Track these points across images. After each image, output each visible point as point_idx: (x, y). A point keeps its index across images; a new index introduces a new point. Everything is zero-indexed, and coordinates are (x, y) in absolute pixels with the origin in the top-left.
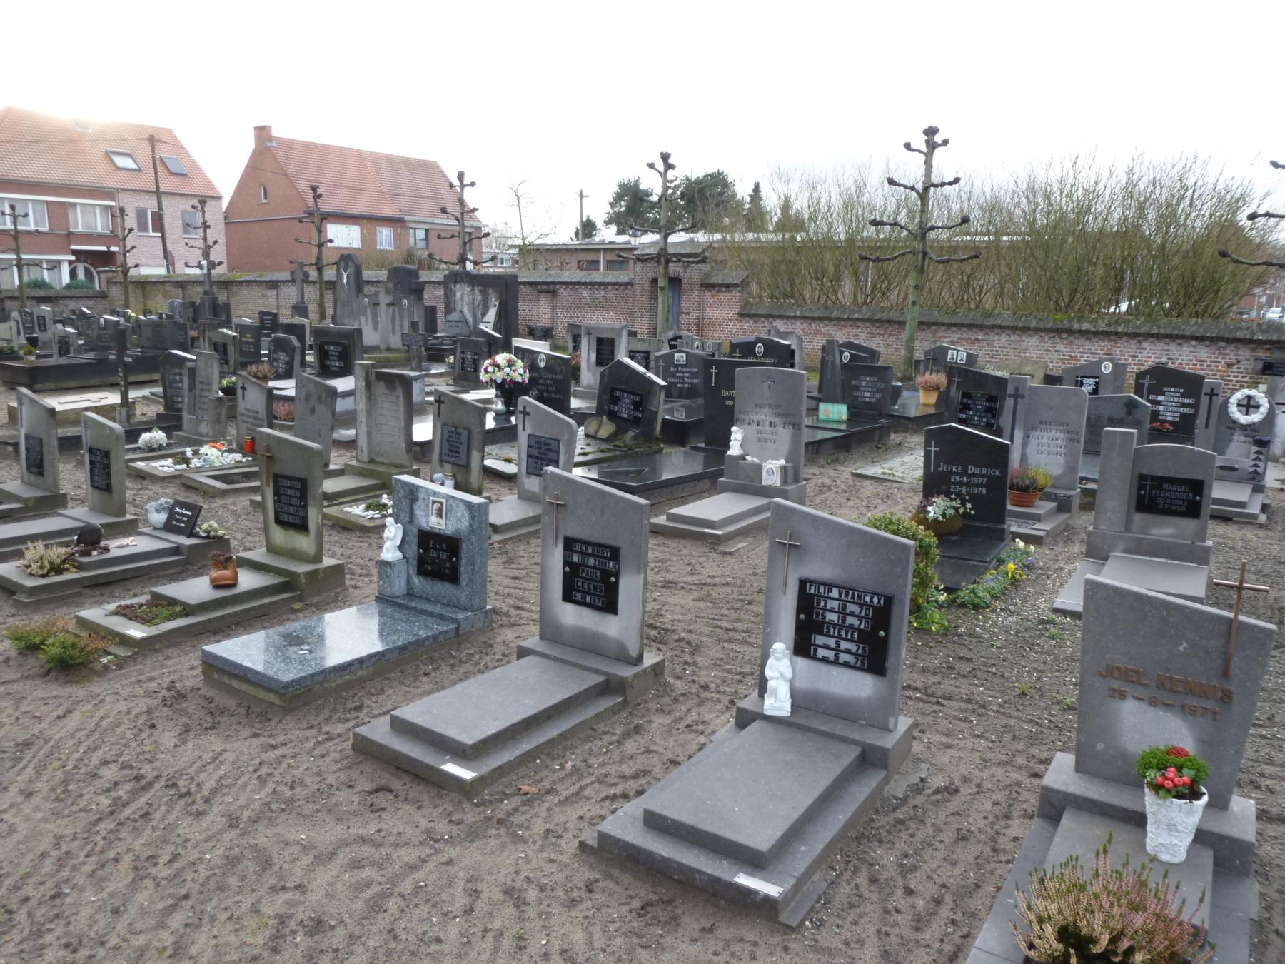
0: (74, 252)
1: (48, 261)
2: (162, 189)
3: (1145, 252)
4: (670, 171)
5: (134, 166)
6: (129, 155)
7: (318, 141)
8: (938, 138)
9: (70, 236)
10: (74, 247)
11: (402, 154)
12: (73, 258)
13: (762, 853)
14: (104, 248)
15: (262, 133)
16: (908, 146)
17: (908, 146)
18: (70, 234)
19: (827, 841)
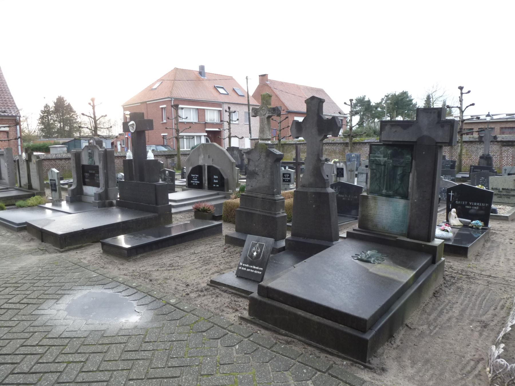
0: (207, 132)
1: (186, 136)
2: (250, 103)
3: (437, 372)
4: (463, 90)
5: (225, 93)
6: (222, 88)
7: (282, 81)
8: (464, 91)
9: (206, 124)
10: (207, 129)
11: (9, 86)
12: (206, 134)
13: (441, 108)
14: (217, 130)
15: (263, 77)
16: (345, 103)
17: (345, 103)
18: (206, 123)
19: (289, 307)
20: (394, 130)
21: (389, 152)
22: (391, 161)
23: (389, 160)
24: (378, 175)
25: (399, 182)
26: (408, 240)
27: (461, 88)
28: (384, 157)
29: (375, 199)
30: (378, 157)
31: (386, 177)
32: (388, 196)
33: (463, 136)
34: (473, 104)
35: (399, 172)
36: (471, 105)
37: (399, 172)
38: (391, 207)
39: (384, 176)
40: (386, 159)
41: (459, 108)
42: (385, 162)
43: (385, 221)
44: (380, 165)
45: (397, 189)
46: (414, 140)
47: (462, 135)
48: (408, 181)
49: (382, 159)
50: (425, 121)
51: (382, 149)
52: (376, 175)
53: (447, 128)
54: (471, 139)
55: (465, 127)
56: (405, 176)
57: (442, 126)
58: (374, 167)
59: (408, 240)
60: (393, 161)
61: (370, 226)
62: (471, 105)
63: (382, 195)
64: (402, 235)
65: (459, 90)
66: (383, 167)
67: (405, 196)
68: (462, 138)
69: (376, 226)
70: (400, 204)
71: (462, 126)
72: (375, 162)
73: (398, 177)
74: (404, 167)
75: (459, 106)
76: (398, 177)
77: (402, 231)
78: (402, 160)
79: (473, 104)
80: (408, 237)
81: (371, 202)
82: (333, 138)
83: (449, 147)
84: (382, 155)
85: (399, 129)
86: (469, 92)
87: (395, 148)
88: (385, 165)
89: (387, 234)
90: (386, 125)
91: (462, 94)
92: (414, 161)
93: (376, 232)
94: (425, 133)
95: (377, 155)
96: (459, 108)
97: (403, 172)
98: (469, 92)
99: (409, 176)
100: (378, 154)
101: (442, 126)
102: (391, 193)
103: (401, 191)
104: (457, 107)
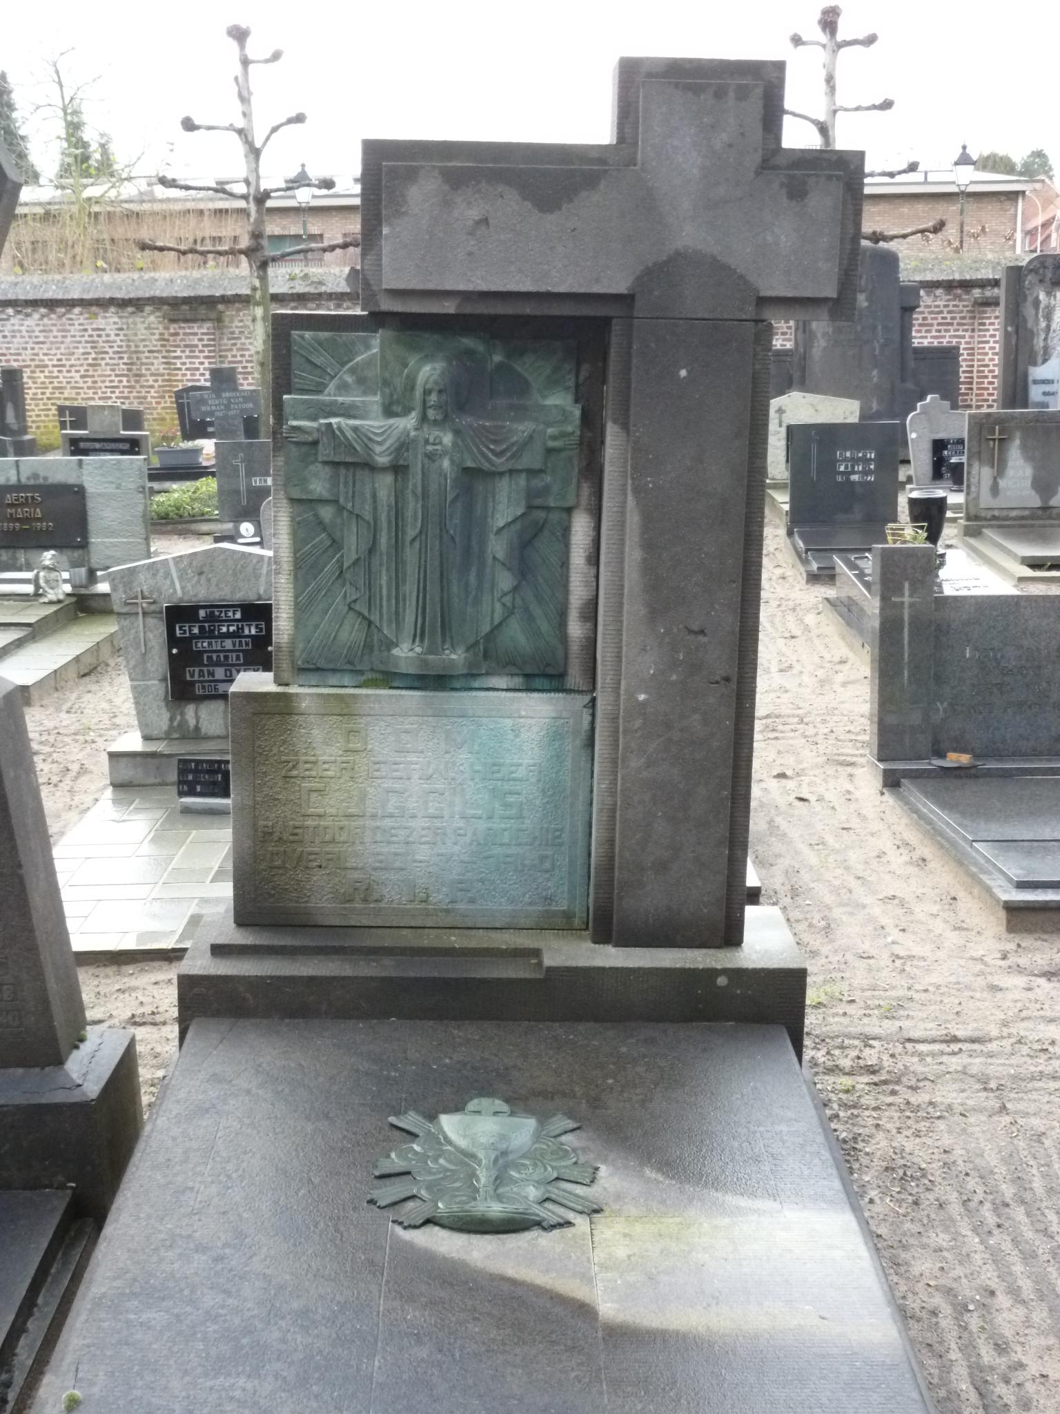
4: (250, 41)
8: (255, 48)
20: (474, 214)
21: (429, 372)
22: (448, 439)
23: (435, 433)
24: (353, 546)
25: (505, 581)
26: (612, 957)
27: (240, 35)
28: (389, 412)
29: (344, 709)
30: (347, 411)
31: (411, 555)
32: (434, 680)
33: (271, 271)
34: (299, 119)
35: (504, 507)
36: (290, 121)
37: (504, 507)
38: (463, 756)
39: (397, 546)
40: (408, 423)
41: (240, 132)
42: (404, 445)
43: (423, 853)
44: (369, 467)
45: (496, 628)
46: (619, 284)
47: (264, 265)
48: (565, 563)
49: (374, 423)
50: (681, 157)
51: (375, 345)
52: (336, 544)
53: (823, 200)
54: (300, 288)
55: (273, 228)
56: (538, 535)
57: (797, 192)
58: (319, 486)
59: (612, 957)
60: (457, 433)
61: (322, 899)
62: (290, 121)
63: (389, 678)
64: (563, 924)
65: (233, 44)
66: (386, 482)
67: (544, 674)
68: (263, 278)
69: (367, 892)
70: (521, 727)
71: (260, 222)
72: (325, 452)
73: (497, 547)
74: (532, 473)
75: (240, 123)
76: (497, 547)
77: (549, 899)
78: (523, 428)
79: (299, 119)
80: (604, 928)
81: (317, 734)
82: (237, 271)
83: (206, 327)
84: (375, 400)
85: (508, 205)
86: (276, 56)
87: (467, 342)
88: (398, 469)
89: (454, 940)
90: (411, 175)
91: (245, 62)
92: (613, 438)
93: (369, 941)
94: (689, 236)
95: (330, 395)
96: (240, 132)
97: (530, 507)
98: (276, 56)
99: (566, 531)
100: (343, 388)
101: (797, 192)
102: (456, 657)
103: (516, 636)
104: (231, 128)
